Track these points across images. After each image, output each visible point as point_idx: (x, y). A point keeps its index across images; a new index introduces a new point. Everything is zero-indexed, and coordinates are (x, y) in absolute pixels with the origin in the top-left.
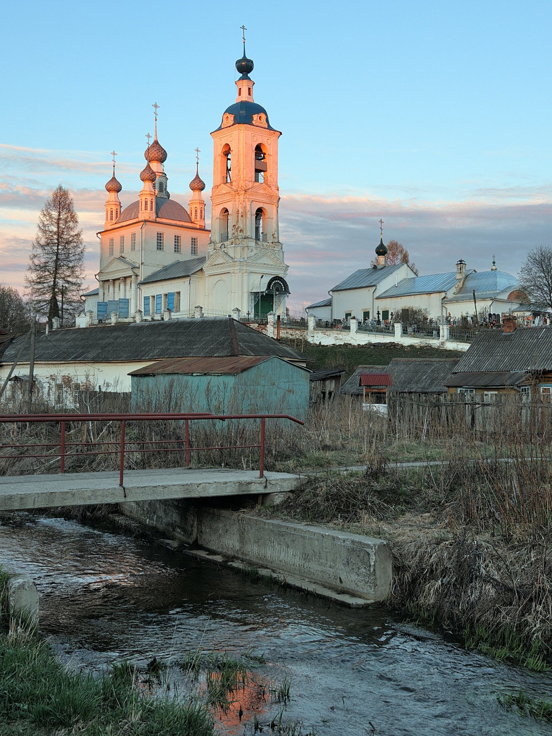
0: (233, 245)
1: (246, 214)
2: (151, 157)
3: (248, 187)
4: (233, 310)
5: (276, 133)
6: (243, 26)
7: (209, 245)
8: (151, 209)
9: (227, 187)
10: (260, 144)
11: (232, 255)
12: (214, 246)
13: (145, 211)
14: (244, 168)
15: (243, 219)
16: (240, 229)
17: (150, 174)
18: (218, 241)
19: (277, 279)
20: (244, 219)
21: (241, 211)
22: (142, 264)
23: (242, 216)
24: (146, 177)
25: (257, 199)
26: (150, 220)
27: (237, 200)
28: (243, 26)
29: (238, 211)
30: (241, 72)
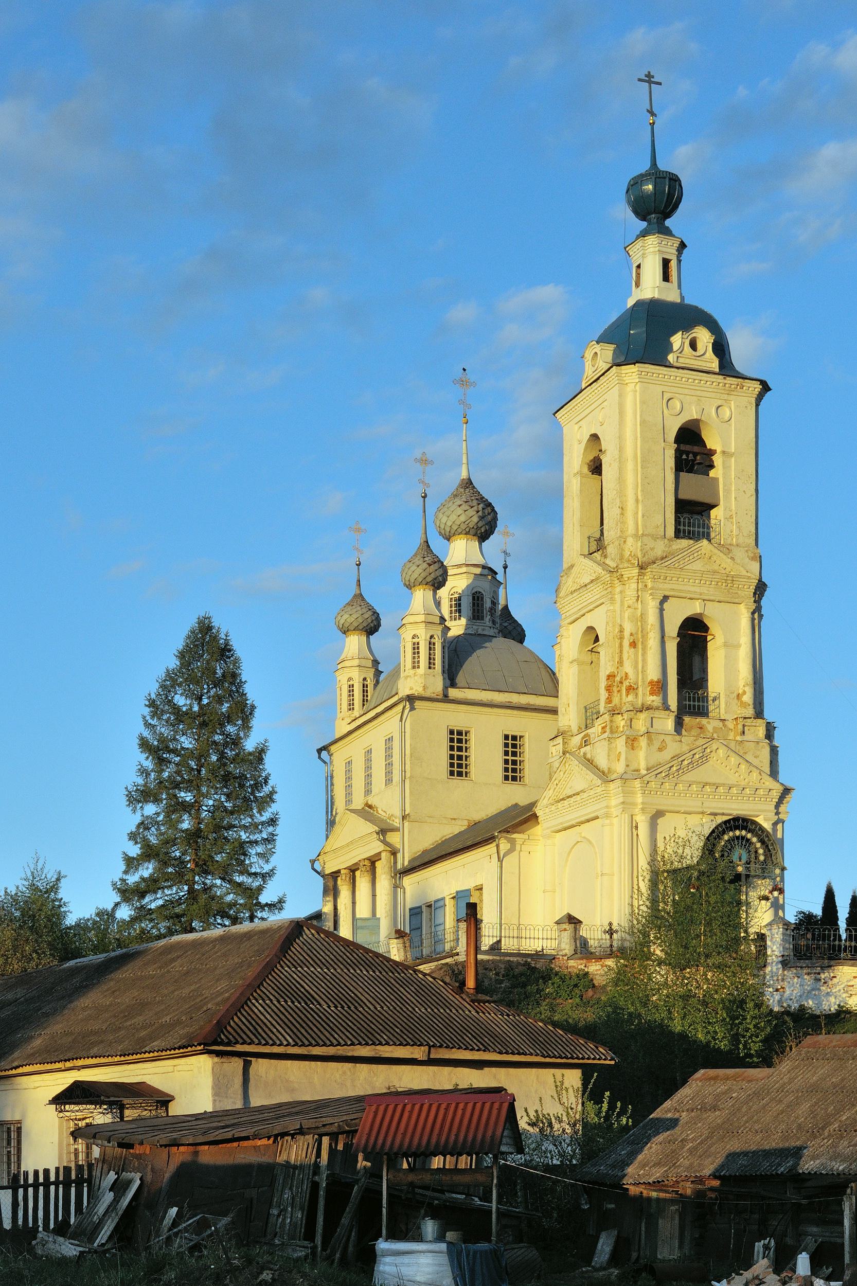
0: (606, 735)
1: (645, 637)
2: (449, 524)
3: (652, 555)
4: (557, 923)
5: (747, 383)
6: (649, 75)
7: (552, 743)
8: (431, 665)
9: (595, 565)
10: (696, 422)
11: (602, 762)
12: (564, 743)
13: (412, 672)
14: (637, 501)
15: (636, 655)
16: (626, 683)
17: (425, 565)
18: (575, 729)
19: (737, 828)
20: (640, 651)
21: (628, 628)
22: (404, 818)
23: (633, 644)
24: (415, 575)
25: (680, 591)
26: (428, 694)
27: (618, 597)
28: (649, 75)
29: (621, 631)
30: (644, 219)
